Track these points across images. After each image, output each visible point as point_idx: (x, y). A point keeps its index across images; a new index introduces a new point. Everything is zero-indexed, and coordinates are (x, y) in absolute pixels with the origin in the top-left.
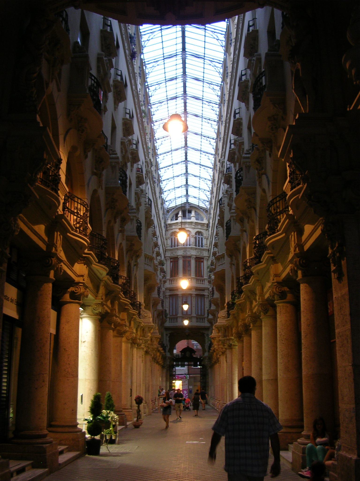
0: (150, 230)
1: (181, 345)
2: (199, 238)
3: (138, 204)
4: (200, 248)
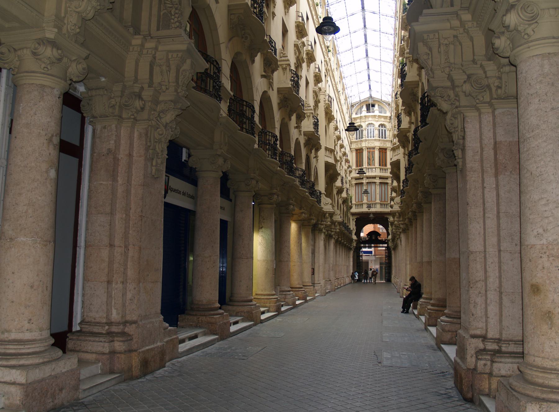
0: (332, 125)
1: (368, 229)
2: (382, 130)
3: (317, 102)
4: (384, 139)
